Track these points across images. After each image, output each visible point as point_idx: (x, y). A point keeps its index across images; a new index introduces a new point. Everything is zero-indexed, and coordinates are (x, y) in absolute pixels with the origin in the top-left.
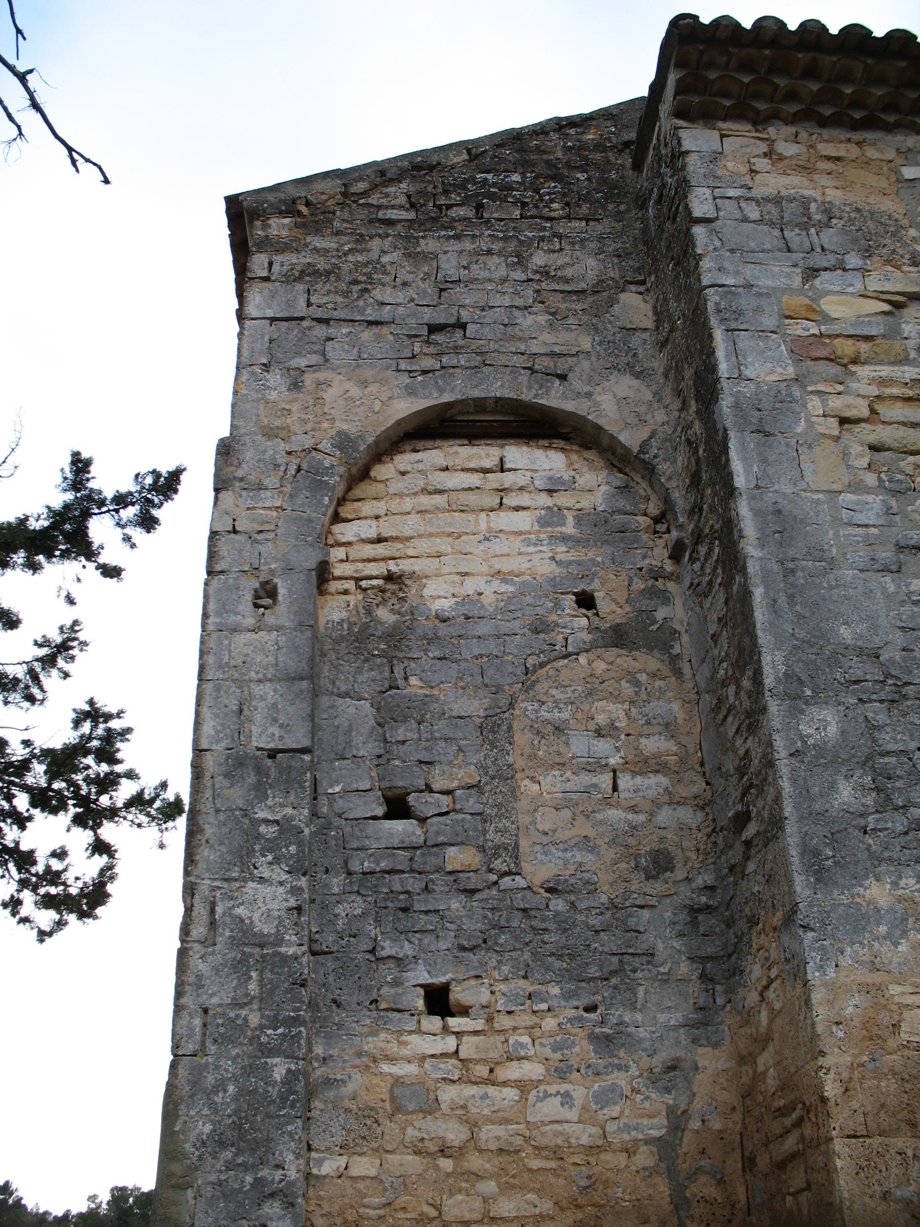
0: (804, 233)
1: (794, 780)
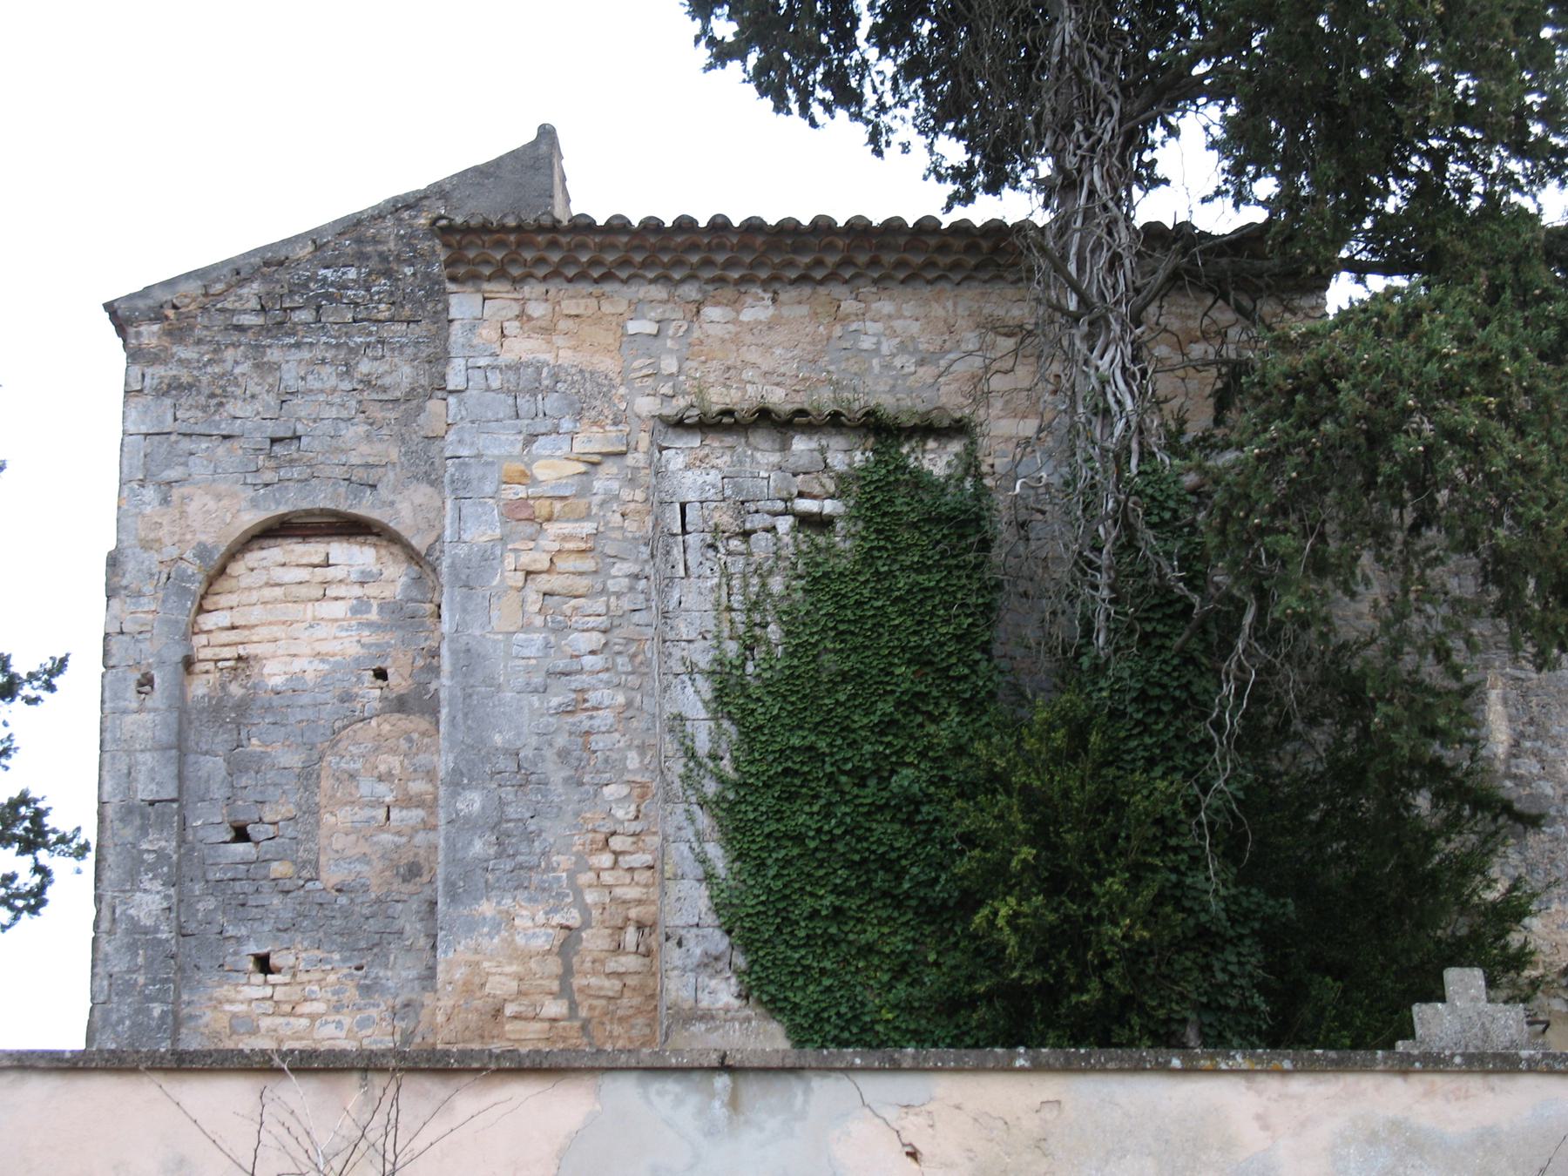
1: (447, 839)
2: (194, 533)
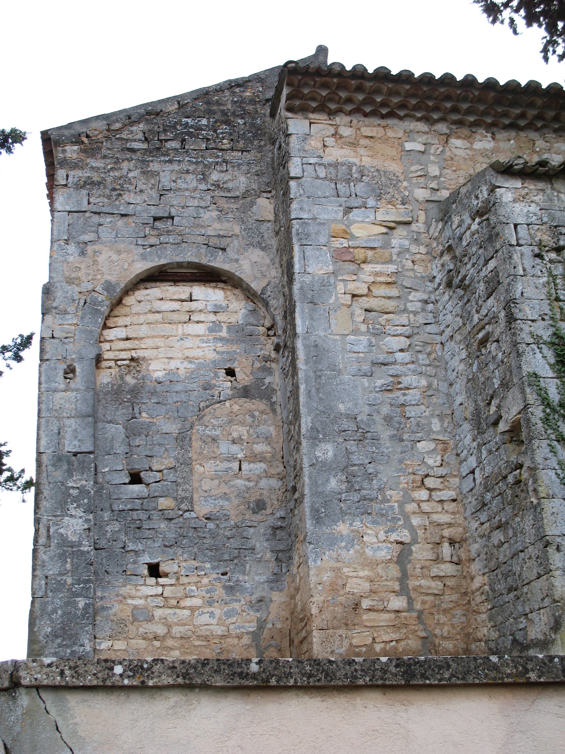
0: (347, 185)
1: (310, 478)
2: (103, 274)
